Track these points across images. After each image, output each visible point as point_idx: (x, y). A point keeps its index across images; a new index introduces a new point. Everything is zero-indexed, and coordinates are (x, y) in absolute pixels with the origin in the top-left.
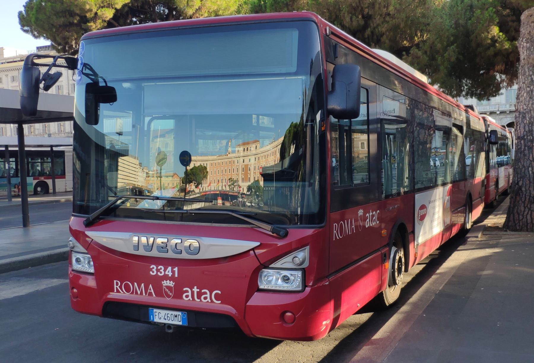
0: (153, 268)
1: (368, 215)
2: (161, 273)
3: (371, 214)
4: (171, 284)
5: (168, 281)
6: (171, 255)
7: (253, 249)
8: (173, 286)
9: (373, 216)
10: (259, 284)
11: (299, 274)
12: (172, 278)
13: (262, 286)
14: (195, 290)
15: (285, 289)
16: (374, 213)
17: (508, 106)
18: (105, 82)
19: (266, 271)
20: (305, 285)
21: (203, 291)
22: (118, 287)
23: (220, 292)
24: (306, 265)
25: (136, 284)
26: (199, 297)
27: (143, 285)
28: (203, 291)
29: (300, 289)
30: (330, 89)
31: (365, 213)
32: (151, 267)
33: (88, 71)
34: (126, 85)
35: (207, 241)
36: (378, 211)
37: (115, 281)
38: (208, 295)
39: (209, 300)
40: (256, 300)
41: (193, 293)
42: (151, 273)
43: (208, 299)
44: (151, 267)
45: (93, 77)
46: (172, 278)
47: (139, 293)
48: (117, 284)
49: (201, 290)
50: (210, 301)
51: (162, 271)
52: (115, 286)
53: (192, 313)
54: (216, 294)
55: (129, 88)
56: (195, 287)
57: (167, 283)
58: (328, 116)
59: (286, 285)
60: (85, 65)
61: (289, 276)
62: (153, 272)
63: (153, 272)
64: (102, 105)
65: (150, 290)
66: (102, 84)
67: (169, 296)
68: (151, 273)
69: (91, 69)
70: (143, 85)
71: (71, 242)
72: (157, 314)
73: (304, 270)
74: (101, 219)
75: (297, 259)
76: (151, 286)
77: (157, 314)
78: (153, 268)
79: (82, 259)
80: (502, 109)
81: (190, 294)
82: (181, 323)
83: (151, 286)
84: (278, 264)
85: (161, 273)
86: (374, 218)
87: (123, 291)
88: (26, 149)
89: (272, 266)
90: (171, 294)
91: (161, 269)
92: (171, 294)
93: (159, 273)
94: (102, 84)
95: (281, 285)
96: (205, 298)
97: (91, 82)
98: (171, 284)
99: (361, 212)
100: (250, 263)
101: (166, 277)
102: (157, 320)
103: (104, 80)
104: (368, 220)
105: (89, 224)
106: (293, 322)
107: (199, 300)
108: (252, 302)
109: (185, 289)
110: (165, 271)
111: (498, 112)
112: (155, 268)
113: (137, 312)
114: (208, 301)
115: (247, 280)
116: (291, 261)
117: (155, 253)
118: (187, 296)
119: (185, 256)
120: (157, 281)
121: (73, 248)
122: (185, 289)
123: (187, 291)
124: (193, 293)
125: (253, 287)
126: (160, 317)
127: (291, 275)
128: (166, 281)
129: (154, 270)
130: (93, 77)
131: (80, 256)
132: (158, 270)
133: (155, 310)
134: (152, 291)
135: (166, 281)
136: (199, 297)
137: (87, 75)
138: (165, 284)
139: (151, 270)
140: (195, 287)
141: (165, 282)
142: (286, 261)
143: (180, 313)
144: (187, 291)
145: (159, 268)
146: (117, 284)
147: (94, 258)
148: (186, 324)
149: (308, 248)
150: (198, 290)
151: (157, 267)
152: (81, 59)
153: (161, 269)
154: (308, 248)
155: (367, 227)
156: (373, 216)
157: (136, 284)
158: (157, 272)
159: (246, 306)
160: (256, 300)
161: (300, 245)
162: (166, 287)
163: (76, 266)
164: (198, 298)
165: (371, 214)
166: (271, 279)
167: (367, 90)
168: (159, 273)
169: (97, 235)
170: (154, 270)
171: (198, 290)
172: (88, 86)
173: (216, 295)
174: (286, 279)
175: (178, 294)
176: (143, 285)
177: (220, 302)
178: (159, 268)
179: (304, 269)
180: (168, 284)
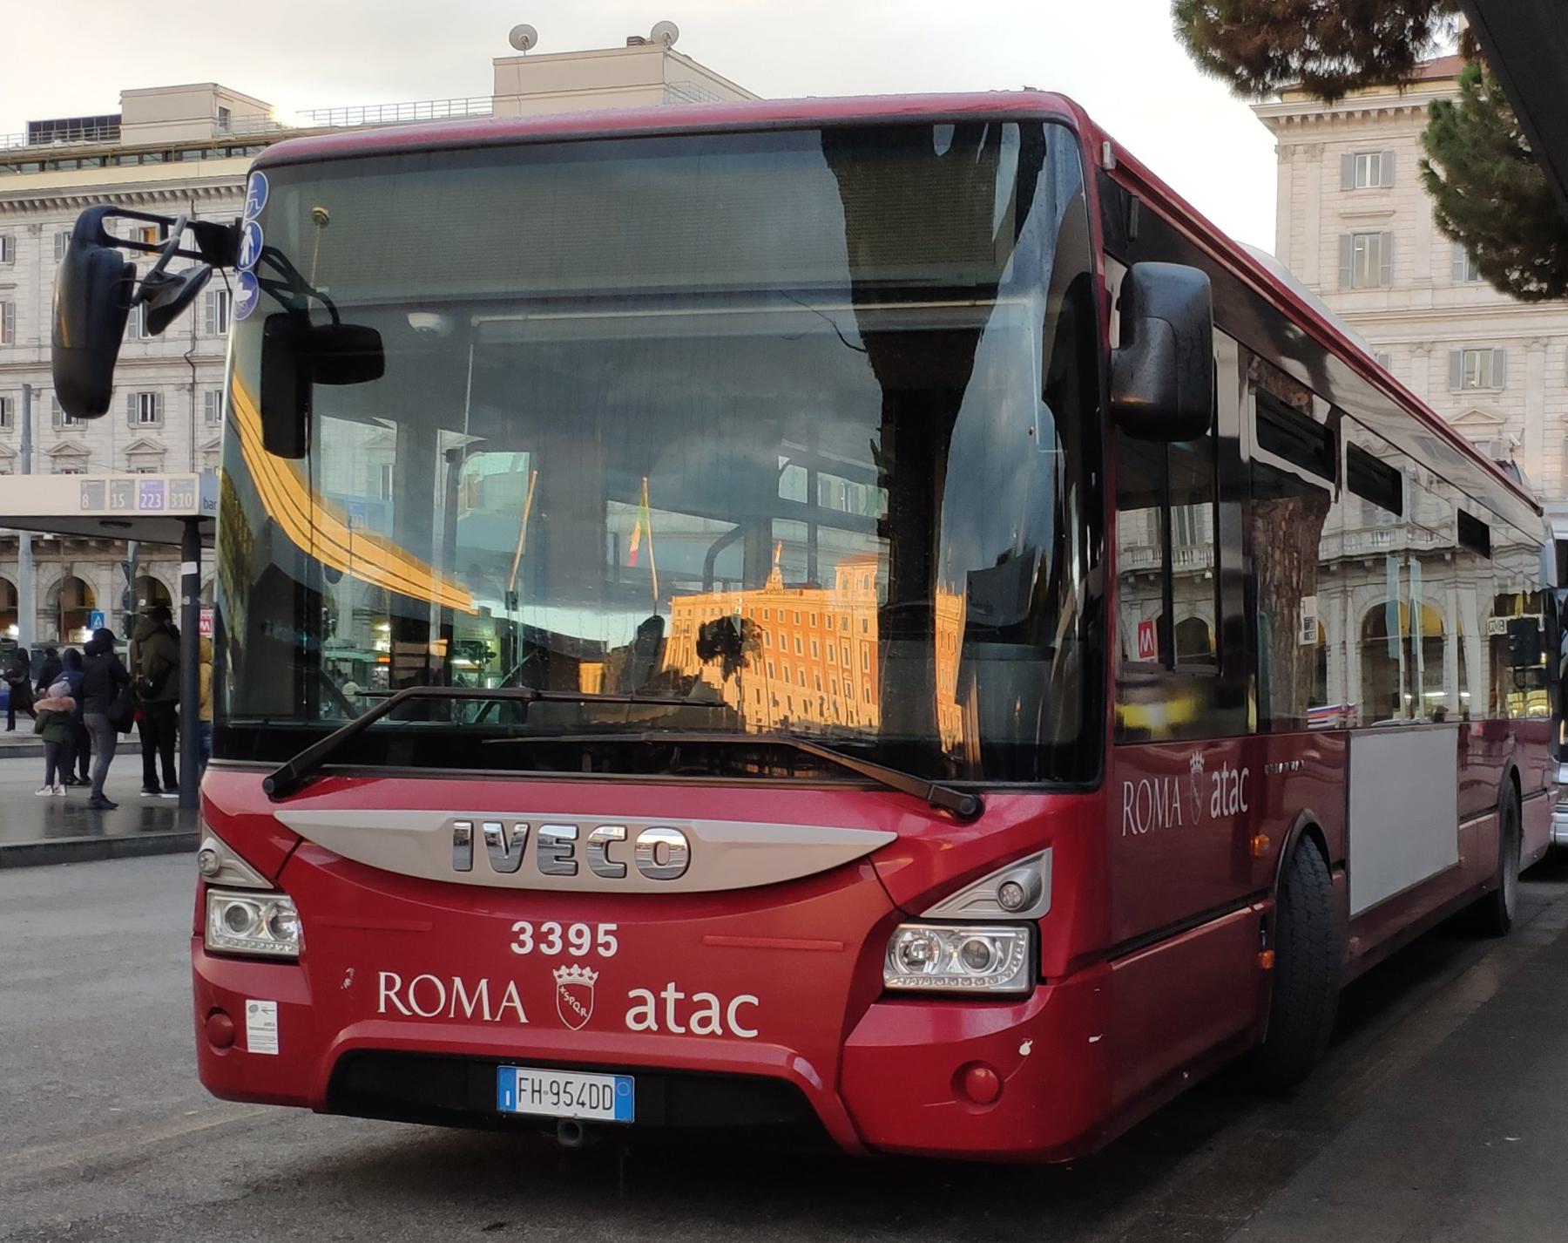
2: (551, 945)
3: (1225, 774)
5: (575, 969)
6: (588, 881)
7: (867, 859)
8: (592, 983)
10: (886, 976)
11: (1021, 937)
14: (671, 994)
15: (974, 987)
18: (333, 310)
19: (908, 934)
20: (1037, 975)
21: (696, 998)
22: (391, 994)
24: (1040, 909)
25: (458, 981)
27: (483, 983)
28: (696, 998)
29: (1022, 986)
32: (516, 928)
34: (422, 321)
35: (710, 831)
37: (383, 975)
38: (714, 1012)
39: (713, 1027)
40: (880, 1029)
42: (515, 947)
44: (516, 928)
45: (289, 295)
46: (591, 960)
47: (469, 1011)
48: (390, 984)
49: (689, 996)
50: (719, 1031)
51: (555, 937)
52: (383, 992)
53: (655, 1081)
55: (431, 332)
56: (671, 986)
57: (565, 976)
59: (974, 973)
61: (986, 942)
62: (522, 944)
63: (522, 944)
64: (321, 392)
65: (510, 999)
66: (320, 320)
68: (515, 947)
69: (287, 269)
70: (475, 320)
71: (209, 856)
72: (526, 1085)
74: (328, 772)
75: (1012, 888)
76: (512, 987)
77: (526, 1085)
79: (250, 913)
81: (650, 1009)
82: (610, 1116)
83: (512, 987)
84: (950, 907)
85: (551, 945)
86: (1235, 791)
87: (409, 1008)
90: (583, 1012)
91: (551, 931)
92: (583, 1012)
93: (543, 947)
94: (320, 320)
96: (705, 1022)
97: (283, 310)
98: (587, 977)
100: (856, 906)
103: (328, 302)
104: (1217, 794)
105: (282, 790)
107: (682, 1030)
109: (632, 994)
112: (529, 929)
114: (713, 1032)
115: (852, 956)
116: (993, 893)
117: (531, 876)
119: (636, 883)
121: (217, 873)
122: (632, 994)
123: (641, 1001)
125: (867, 988)
126: (535, 1094)
127: (993, 940)
128: (569, 967)
129: (526, 937)
130: (289, 295)
132: (539, 937)
133: (521, 1073)
134: (517, 1003)
135: (569, 967)
136: (682, 1019)
137: (266, 285)
138: (566, 980)
139: (515, 937)
140: (671, 986)
141: (564, 970)
142: (979, 898)
143: (610, 1080)
144: (641, 1001)
145: (544, 928)
146: (390, 984)
148: (629, 1117)
149: (1047, 853)
150: (681, 996)
151: (536, 926)
152: (255, 234)
154: (1047, 853)
155: (1214, 815)
156: (1231, 783)
157: (458, 981)
158: (536, 946)
159: (842, 1047)
160: (880, 1029)
161: (1019, 844)
162: (567, 986)
164: (678, 1023)
165: (1225, 774)
166: (929, 958)
168: (543, 947)
169: (331, 822)
170: (526, 937)
171: (681, 996)
172: (272, 321)
173: (743, 1010)
174: (981, 958)
176: (483, 983)
177: (754, 1033)
178: (544, 928)
179: (1035, 921)
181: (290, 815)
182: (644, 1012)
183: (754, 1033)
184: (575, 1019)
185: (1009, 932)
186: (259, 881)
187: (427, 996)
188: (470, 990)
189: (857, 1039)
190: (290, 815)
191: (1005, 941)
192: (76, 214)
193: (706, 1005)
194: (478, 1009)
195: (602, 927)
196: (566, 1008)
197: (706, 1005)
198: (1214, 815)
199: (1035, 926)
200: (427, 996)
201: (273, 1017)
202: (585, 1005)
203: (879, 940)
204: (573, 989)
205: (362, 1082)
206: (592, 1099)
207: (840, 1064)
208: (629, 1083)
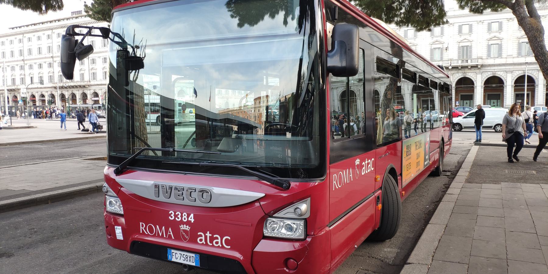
0: (172, 213)
1: (364, 163)
2: (178, 218)
3: (366, 162)
4: (187, 228)
5: (185, 226)
9: (368, 164)
11: (302, 223)
12: (188, 223)
13: (267, 233)
14: (208, 235)
16: (369, 161)
17: (460, 62)
19: (270, 219)
21: (215, 236)
23: (229, 238)
24: (307, 216)
25: (158, 226)
26: (211, 242)
28: (215, 236)
29: (303, 237)
30: (330, 48)
31: (361, 162)
33: (117, 39)
36: (373, 159)
38: (219, 240)
39: (220, 246)
40: (263, 247)
41: (206, 237)
43: (219, 244)
48: (143, 226)
53: (204, 257)
54: (226, 240)
56: (208, 232)
57: (184, 227)
58: (328, 75)
60: (116, 34)
62: (172, 217)
63: (172, 217)
67: (185, 239)
69: (120, 37)
72: (174, 254)
73: (306, 220)
74: (128, 168)
75: (298, 210)
76: (170, 229)
77: (174, 254)
78: (172, 213)
80: (455, 64)
81: (203, 238)
82: (194, 264)
83: (170, 229)
84: (281, 214)
85: (178, 218)
86: (370, 165)
88: (193, 81)
89: (276, 215)
91: (178, 214)
95: (284, 233)
96: (217, 243)
98: (187, 228)
99: (357, 162)
100: (256, 213)
101: (182, 222)
102: (174, 260)
104: (364, 168)
105: (118, 172)
106: (295, 269)
108: (258, 249)
109: (199, 233)
110: (182, 216)
111: (450, 67)
113: (159, 252)
116: (293, 211)
118: (201, 240)
120: (175, 225)
122: (199, 233)
124: (206, 237)
126: (177, 257)
129: (172, 215)
131: (112, 200)
132: (176, 216)
133: (173, 251)
134: (172, 234)
136: (211, 242)
137: (117, 43)
138: (183, 228)
139: (170, 215)
140: (208, 232)
141: (182, 226)
143: (194, 255)
144: (201, 236)
145: (177, 214)
146: (143, 226)
147: (123, 203)
148: (199, 265)
151: (175, 213)
153: (178, 214)
155: (363, 174)
156: (368, 164)
157: (158, 226)
162: (183, 230)
163: (109, 208)
164: (210, 242)
165: (366, 162)
167: (363, 50)
170: (172, 215)
174: (289, 228)
175: (193, 239)
177: (229, 247)
178: (177, 214)
180: (185, 228)
181: (120, 179)
182: (202, 237)
183: (229, 247)
184: (185, 239)
185: (298, 222)
186: (115, 195)
187: (151, 230)
188: (161, 229)
189: (257, 249)
190: (120, 179)
191: (297, 225)
192: (65, 29)
193: (217, 238)
194: (163, 234)
195: (173, 218)
196: (183, 235)
197: (217, 238)
198: (363, 174)
199: (306, 220)
200: (151, 230)
201: (121, 231)
202: (187, 235)
203: (262, 222)
204: (185, 231)
205: (138, 247)
206: (191, 260)
207: (253, 256)
208: (198, 256)
